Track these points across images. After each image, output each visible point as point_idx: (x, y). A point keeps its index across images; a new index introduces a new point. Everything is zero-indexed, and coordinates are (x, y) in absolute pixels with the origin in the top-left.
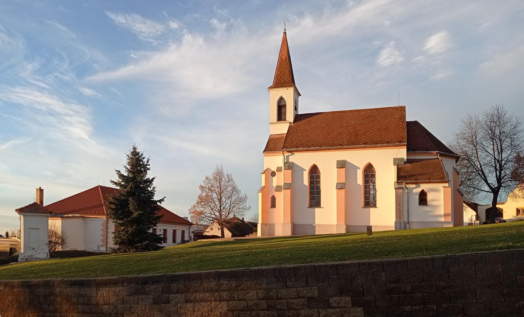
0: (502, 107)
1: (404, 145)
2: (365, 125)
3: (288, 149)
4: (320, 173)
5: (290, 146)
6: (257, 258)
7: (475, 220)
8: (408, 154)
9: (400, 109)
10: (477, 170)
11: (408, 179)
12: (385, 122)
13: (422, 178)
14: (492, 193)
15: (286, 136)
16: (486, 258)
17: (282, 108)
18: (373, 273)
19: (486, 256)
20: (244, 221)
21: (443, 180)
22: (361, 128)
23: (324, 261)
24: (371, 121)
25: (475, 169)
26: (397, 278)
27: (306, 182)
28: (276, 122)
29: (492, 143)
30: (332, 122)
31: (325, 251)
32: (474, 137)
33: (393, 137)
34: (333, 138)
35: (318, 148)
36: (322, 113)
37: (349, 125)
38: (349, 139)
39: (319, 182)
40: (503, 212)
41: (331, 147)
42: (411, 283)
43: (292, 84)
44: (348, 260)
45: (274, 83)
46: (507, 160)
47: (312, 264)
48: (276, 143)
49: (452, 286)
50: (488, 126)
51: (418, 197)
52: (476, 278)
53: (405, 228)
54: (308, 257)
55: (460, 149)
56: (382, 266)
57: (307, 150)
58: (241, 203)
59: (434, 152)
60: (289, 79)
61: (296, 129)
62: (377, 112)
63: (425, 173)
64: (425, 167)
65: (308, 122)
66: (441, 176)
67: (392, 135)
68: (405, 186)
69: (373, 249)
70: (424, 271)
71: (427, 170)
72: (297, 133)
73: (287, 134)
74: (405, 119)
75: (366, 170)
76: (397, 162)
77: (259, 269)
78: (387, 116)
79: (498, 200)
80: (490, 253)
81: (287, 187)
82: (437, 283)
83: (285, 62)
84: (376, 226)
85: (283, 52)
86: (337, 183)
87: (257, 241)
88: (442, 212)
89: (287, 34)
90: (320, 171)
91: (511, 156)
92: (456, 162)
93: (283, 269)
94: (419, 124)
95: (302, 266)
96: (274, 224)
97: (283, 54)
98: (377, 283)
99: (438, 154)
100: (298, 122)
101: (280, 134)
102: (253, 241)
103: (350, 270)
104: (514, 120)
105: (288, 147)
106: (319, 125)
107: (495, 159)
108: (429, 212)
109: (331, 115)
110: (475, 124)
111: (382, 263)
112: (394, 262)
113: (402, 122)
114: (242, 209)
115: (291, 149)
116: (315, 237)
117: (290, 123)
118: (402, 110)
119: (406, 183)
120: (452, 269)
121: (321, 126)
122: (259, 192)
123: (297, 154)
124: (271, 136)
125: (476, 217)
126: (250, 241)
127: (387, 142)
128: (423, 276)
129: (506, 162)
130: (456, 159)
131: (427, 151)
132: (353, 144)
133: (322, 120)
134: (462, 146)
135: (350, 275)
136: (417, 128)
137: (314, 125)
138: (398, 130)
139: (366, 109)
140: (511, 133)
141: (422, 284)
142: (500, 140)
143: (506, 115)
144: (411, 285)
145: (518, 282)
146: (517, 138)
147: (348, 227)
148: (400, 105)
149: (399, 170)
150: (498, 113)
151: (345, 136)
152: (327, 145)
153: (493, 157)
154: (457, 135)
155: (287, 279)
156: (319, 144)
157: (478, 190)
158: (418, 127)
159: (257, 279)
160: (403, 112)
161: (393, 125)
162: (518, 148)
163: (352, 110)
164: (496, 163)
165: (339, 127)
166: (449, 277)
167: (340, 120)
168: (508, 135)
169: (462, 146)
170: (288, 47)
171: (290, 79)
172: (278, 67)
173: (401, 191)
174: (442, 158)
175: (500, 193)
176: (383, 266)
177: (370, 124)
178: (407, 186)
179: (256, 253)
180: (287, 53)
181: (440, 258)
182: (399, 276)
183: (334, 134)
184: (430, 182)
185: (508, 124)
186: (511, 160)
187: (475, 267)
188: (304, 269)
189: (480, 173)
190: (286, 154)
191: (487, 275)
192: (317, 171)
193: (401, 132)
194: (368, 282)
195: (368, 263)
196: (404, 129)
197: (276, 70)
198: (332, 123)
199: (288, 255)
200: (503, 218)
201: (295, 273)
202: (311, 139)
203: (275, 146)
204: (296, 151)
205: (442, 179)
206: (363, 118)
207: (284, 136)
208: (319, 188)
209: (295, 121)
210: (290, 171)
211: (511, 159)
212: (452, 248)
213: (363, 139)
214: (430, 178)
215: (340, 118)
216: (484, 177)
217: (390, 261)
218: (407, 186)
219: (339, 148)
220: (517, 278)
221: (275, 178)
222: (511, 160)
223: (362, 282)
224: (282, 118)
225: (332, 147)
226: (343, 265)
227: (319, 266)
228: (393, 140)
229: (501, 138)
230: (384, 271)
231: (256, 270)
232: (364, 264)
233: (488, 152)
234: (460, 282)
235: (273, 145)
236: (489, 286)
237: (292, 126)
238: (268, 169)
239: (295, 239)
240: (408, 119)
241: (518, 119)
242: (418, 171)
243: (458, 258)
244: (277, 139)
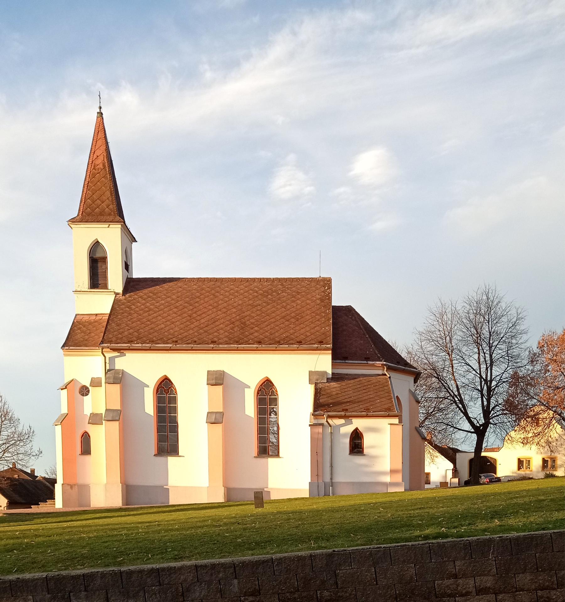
0: (494, 288)
1: (327, 349)
2: (259, 308)
3: (112, 345)
4: (176, 392)
5: (117, 338)
6: (27, 557)
7: (451, 477)
8: (334, 365)
9: (322, 283)
10: (451, 395)
11: (333, 409)
12: (295, 305)
13: (356, 408)
14: (475, 435)
15: (109, 318)
16: (392, 555)
17: (99, 264)
18: (220, 581)
19: (391, 551)
20: (36, 475)
21: (389, 413)
22: (252, 312)
23: (148, 562)
24: (271, 302)
25: (449, 393)
26: (257, 588)
27: (150, 407)
28: (87, 290)
29: (476, 350)
30: (198, 297)
31: (154, 542)
32: (448, 338)
33: (308, 334)
34: (199, 327)
35: (171, 345)
36: (179, 278)
37: (230, 307)
38: (230, 332)
39: (175, 410)
40: (496, 464)
41: (195, 345)
42: (278, 594)
43: (118, 218)
44: (189, 558)
45: (81, 213)
46: (500, 380)
47: (115, 569)
48: (88, 331)
49: (341, 598)
50: (470, 321)
51: (348, 440)
52: (377, 584)
53: (326, 494)
54: (121, 554)
55: (425, 358)
56: (233, 568)
57: (150, 349)
58: (22, 444)
59: (378, 363)
60: (111, 207)
61: (129, 307)
62: (282, 285)
63: (361, 399)
64: (362, 388)
65: (151, 295)
66: (386, 406)
67: (308, 328)
68: (327, 421)
69: (236, 538)
70: (298, 576)
71: (365, 394)
72: (130, 314)
73: (110, 315)
74: (331, 303)
75: (260, 390)
76: (315, 377)
77: (19, 578)
78: (298, 293)
79: (484, 445)
80: (398, 546)
81: (112, 417)
82: (318, 593)
83: (101, 173)
84: (278, 490)
85: (98, 153)
86: (208, 413)
87: (52, 517)
88: (387, 467)
89: (104, 116)
90: (175, 389)
91: (506, 373)
92: (415, 382)
93: (64, 577)
94: (354, 312)
95: (97, 572)
97: (98, 156)
98: (225, 596)
99: (385, 367)
100: (132, 293)
101: (96, 315)
102: (43, 518)
103: (182, 577)
104: (513, 312)
105: (112, 341)
106: (173, 301)
107: (481, 377)
108: (366, 466)
109: (195, 285)
110: (449, 316)
111: (233, 565)
112: (252, 562)
113: (324, 306)
114: (25, 454)
115: (119, 345)
116: (165, 509)
117: (117, 294)
118: (326, 283)
119: (329, 417)
120: (341, 572)
121: (177, 304)
122: (56, 424)
123: (130, 356)
124: (78, 316)
125: (453, 472)
126: (38, 518)
127: (297, 342)
128: (297, 582)
129: (498, 383)
130: (415, 377)
131: (367, 361)
132: (237, 342)
133: (179, 294)
134: (428, 353)
135: (182, 584)
136: (351, 318)
137: (163, 302)
138: (318, 320)
139: (261, 279)
140: (508, 334)
141: (296, 596)
142: (489, 347)
143: (500, 304)
144: (278, 597)
145: (437, 590)
146: (517, 344)
147: (229, 492)
148: (323, 275)
149: (318, 393)
150: (488, 299)
151: (221, 325)
152: (189, 341)
153: (477, 374)
154: (421, 334)
155: (71, 594)
156: (174, 339)
157: (452, 429)
158: (354, 318)
159: (15, 597)
160: (327, 289)
161: (309, 312)
162: (519, 360)
163: (235, 278)
164: (483, 384)
165: (210, 307)
166: (337, 583)
167: (213, 295)
168: (502, 338)
169: (428, 353)
170: (107, 143)
171: (113, 207)
172: (87, 180)
173: (320, 430)
174: (389, 373)
175: (487, 434)
176: (235, 569)
177: (269, 307)
178: (330, 421)
179: (29, 546)
180: (105, 155)
181: (323, 555)
182: (260, 584)
183: (202, 321)
184: (369, 415)
185: (503, 319)
186: (507, 379)
187: (375, 568)
188: (102, 578)
189: (456, 399)
190: (110, 354)
191: (393, 581)
192: (170, 388)
193: (323, 325)
194: (211, 595)
195: (211, 565)
196: (329, 320)
197: (84, 187)
198: (198, 300)
199: (85, 551)
200: (496, 474)
201: (85, 584)
202: (157, 329)
203: (87, 337)
204: (129, 349)
205: (388, 413)
206: (255, 294)
207: (104, 318)
208: (174, 421)
209: (126, 290)
210: (117, 387)
211: (506, 378)
212: (357, 535)
213: (256, 334)
214: (369, 409)
215: (213, 292)
216: (463, 407)
217: (245, 562)
218: (330, 421)
219: (211, 348)
220: (436, 584)
221: (87, 399)
222: (507, 379)
223: (202, 596)
224: (100, 282)
225: (198, 346)
226: (170, 569)
227: (127, 572)
228: (308, 339)
229: (491, 342)
230: (236, 576)
231: (13, 581)
232: (205, 566)
233: (470, 366)
234: (353, 591)
235: (83, 334)
236: (395, 596)
237: (120, 300)
238: (73, 380)
239: (127, 513)
240: (336, 302)
241: (519, 312)
242: (351, 395)
243: (350, 554)
244: (90, 323)
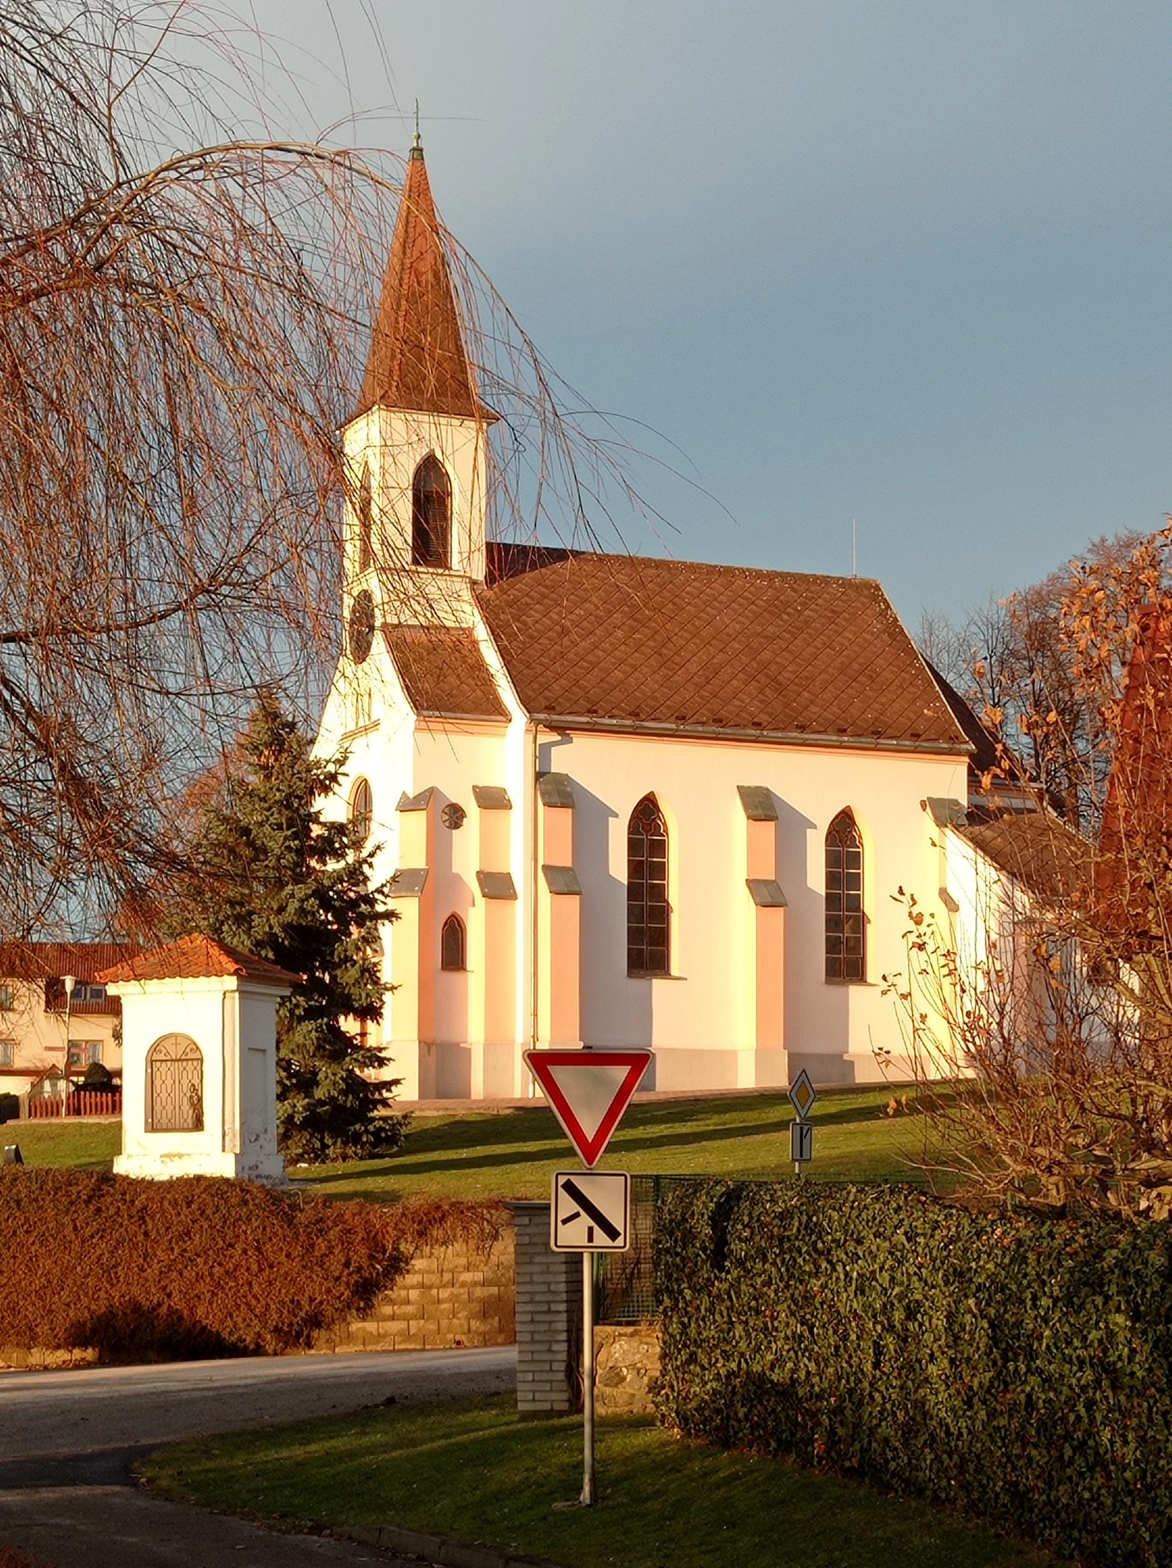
4: (666, 831)
96: (458, 1044)
123: (582, 743)
